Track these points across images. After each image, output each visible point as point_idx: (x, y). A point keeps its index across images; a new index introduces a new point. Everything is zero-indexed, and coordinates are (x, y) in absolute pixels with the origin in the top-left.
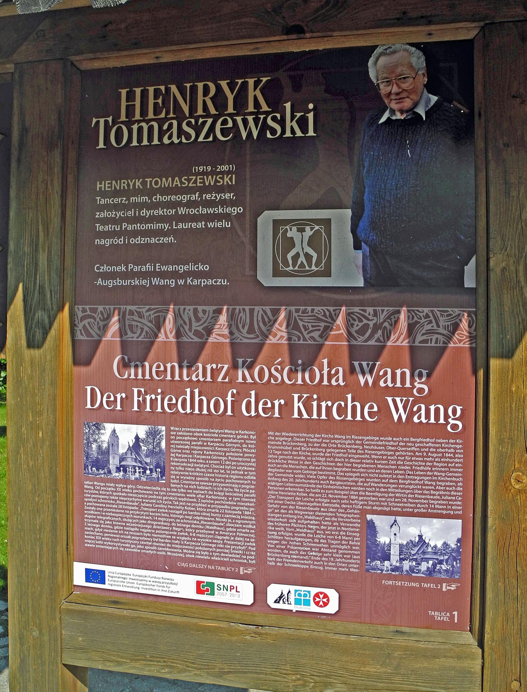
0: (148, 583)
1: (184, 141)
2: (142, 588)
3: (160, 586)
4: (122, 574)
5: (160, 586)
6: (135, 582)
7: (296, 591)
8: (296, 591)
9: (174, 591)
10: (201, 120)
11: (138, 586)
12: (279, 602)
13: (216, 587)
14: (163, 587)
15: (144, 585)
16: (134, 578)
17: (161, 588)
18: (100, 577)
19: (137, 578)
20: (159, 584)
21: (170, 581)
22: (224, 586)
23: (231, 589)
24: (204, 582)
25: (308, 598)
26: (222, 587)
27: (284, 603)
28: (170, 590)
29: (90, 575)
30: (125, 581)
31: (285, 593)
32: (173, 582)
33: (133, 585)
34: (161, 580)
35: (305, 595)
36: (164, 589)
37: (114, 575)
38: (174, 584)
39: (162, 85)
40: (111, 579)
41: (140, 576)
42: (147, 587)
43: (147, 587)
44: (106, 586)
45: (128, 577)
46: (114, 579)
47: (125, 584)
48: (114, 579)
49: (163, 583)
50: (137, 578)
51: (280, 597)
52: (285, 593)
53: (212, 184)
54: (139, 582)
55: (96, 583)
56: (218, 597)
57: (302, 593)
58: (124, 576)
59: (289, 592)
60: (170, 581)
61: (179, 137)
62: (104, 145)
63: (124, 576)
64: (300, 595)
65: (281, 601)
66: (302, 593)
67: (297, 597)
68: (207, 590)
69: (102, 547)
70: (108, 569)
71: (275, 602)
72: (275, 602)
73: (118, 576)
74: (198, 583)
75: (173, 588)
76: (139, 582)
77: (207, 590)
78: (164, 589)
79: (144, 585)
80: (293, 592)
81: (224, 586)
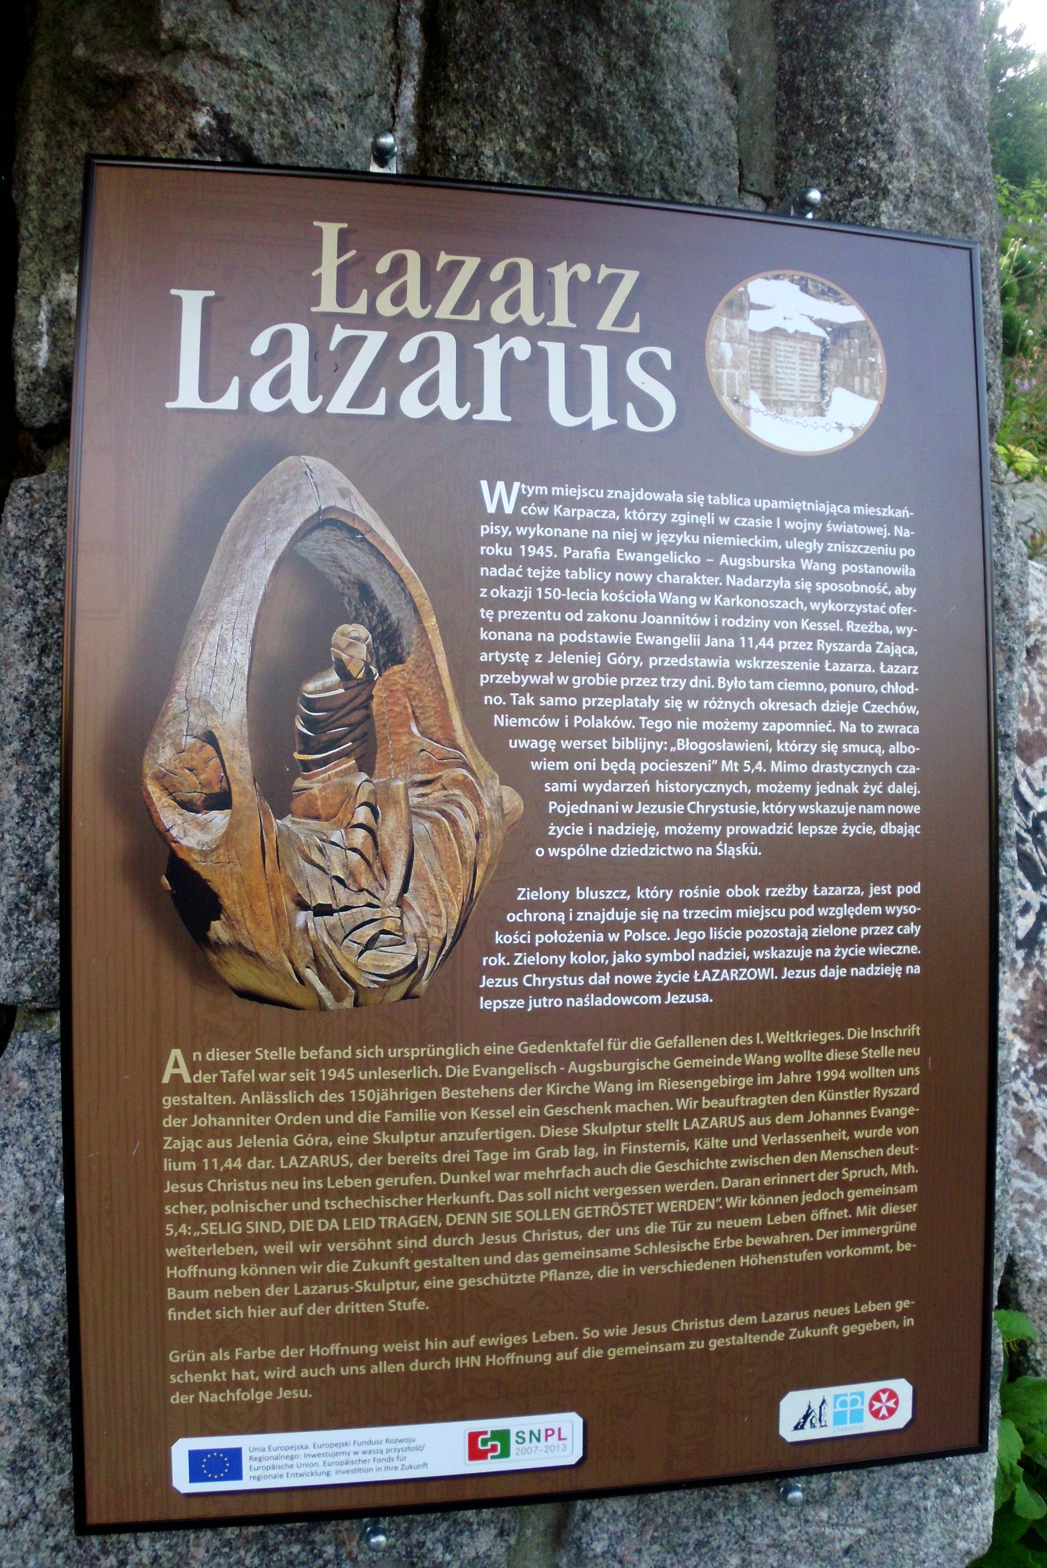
0: (353, 1457)
1: (633, 422)
2: (337, 1472)
3: (381, 1460)
4: (286, 1448)
5: (381, 1460)
6: (320, 1460)
7: (836, 1397)
8: (836, 1397)
9: (415, 1463)
10: (340, 334)
11: (327, 1469)
12: (802, 1427)
13: (513, 1438)
14: (390, 1459)
15: (341, 1464)
16: (317, 1451)
17: (383, 1465)
18: (229, 1464)
19: (323, 1450)
20: (379, 1456)
21: (404, 1445)
22: (531, 1433)
23: (547, 1436)
24: (485, 1433)
25: (858, 1407)
26: (527, 1436)
27: (813, 1426)
28: (407, 1463)
29: (202, 1465)
30: (294, 1462)
31: (815, 1407)
32: (412, 1445)
33: (313, 1469)
34: (384, 1446)
35: (854, 1402)
36: (390, 1464)
37: (267, 1453)
38: (417, 1449)
39: (436, 257)
40: (256, 1464)
41: (331, 1446)
42: (350, 1467)
43: (350, 1467)
44: (246, 1483)
45: (301, 1452)
46: (265, 1463)
47: (295, 1470)
48: (265, 1463)
49: (388, 1451)
50: (323, 1450)
51: (806, 1417)
52: (815, 1407)
53: (509, 509)
54: (330, 1460)
55: (220, 1479)
56: (520, 1459)
57: (849, 1399)
58: (290, 1452)
59: (824, 1401)
60: (404, 1445)
61: (615, 409)
62: (505, 410)
63: (290, 1452)
64: (844, 1403)
65: (808, 1424)
66: (849, 1399)
67: (839, 1409)
68: (494, 1448)
69: (756, 1339)
70: (245, 1442)
71: (796, 1428)
72: (796, 1428)
73: (274, 1454)
74: (473, 1437)
75: (413, 1458)
76: (330, 1460)
77: (494, 1448)
78: (390, 1464)
79: (341, 1464)
80: (830, 1401)
81: (531, 1433)
